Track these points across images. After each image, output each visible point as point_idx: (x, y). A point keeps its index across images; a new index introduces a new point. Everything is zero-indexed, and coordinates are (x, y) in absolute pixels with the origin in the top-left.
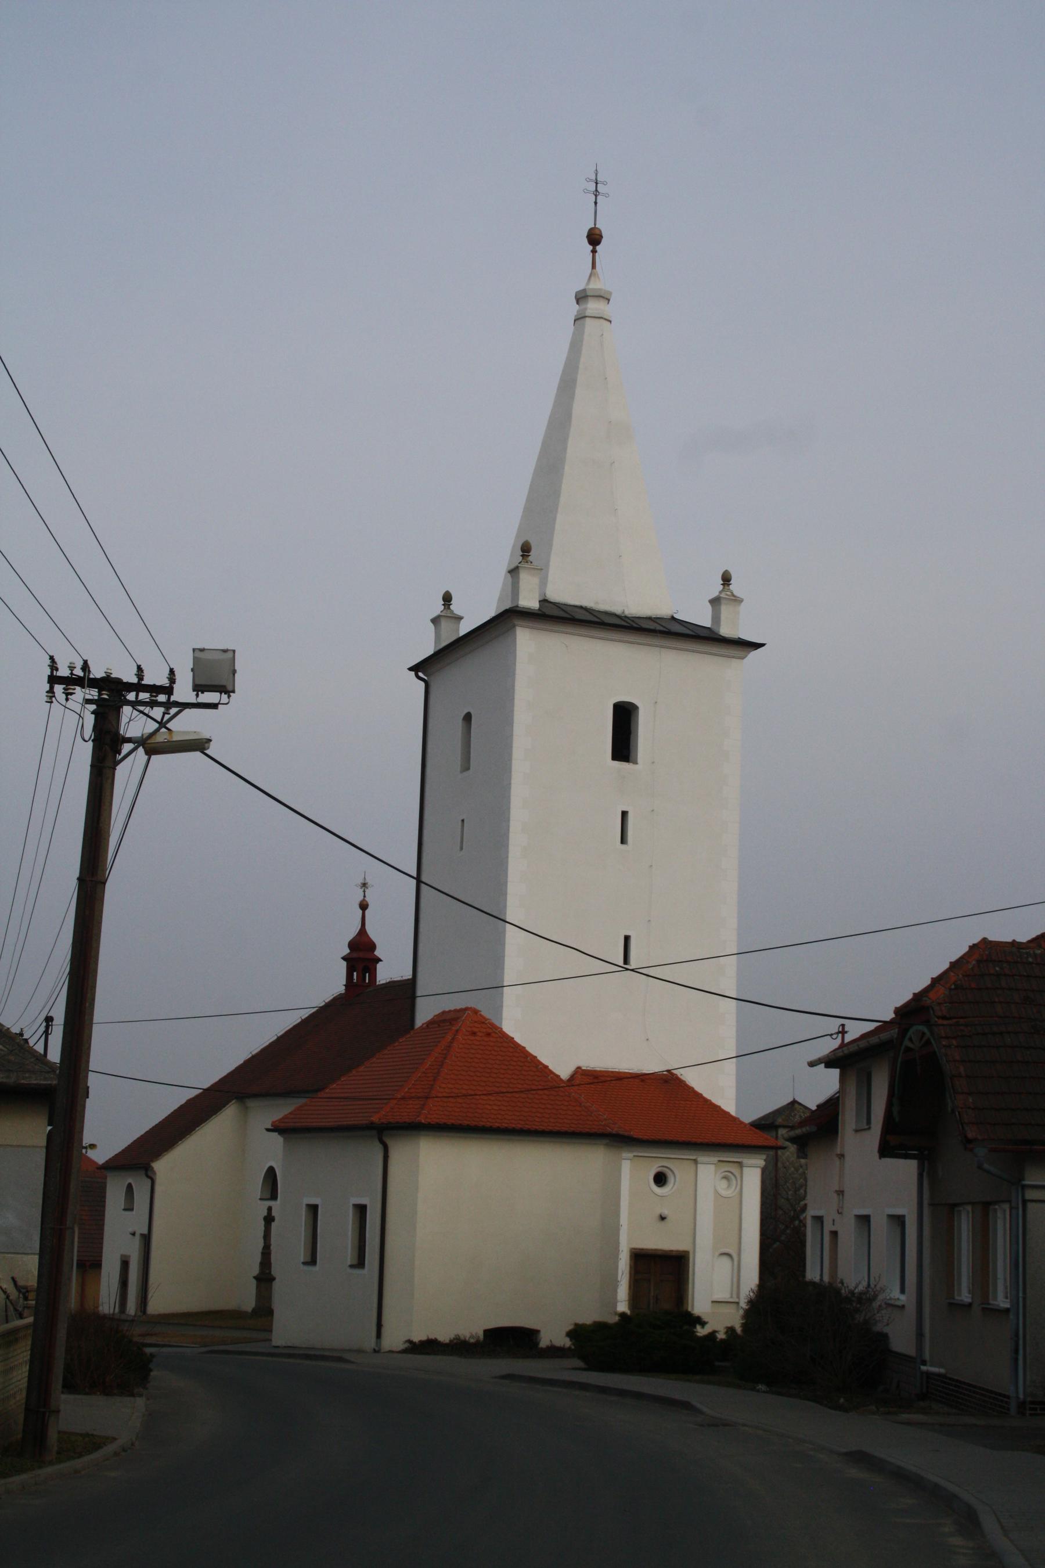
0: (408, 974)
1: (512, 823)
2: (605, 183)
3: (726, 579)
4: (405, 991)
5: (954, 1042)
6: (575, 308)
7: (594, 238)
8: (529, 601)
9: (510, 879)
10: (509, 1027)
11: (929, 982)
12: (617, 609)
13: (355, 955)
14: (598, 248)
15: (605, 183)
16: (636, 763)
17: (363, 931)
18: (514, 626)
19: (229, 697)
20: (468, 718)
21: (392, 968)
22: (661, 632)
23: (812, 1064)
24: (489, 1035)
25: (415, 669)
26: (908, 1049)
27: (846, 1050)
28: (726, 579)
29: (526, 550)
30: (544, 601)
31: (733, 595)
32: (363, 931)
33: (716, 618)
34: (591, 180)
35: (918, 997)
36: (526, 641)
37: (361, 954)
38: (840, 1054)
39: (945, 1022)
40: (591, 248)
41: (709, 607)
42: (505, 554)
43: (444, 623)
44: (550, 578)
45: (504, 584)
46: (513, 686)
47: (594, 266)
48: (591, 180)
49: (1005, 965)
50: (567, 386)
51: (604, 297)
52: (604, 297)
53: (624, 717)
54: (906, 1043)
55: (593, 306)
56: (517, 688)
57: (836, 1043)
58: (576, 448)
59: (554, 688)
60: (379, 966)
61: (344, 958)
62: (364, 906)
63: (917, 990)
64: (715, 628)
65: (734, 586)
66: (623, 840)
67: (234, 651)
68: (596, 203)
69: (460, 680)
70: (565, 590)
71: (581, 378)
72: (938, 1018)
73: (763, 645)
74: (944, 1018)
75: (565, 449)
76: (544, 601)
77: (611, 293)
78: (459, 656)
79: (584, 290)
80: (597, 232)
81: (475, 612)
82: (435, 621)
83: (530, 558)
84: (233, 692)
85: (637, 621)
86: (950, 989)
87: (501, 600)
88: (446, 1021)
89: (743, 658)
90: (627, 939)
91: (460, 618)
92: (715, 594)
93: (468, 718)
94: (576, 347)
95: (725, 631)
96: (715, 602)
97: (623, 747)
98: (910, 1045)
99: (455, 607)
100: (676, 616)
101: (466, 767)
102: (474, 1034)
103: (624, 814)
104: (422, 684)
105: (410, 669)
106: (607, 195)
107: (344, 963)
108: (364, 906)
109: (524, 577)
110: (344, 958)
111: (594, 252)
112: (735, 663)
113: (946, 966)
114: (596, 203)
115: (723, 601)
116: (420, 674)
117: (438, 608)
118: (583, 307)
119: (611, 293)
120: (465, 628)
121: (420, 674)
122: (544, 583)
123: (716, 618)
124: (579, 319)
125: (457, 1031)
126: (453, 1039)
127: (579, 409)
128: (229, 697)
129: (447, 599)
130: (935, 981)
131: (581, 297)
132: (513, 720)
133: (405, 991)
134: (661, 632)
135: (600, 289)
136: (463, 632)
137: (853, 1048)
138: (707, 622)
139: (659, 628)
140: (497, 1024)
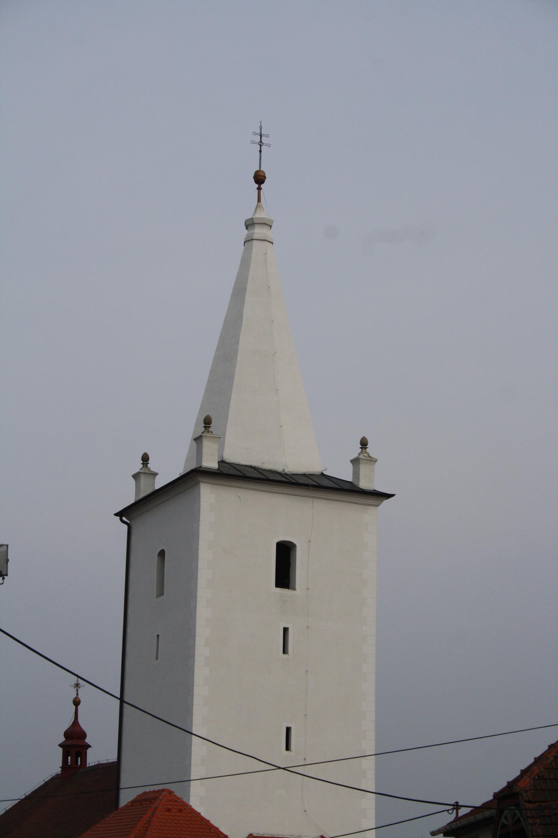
0: (113, 757)
1: (197, 639)
2: (267, 136)
3: (364, 444)
4: (112, 772)
5: (538, 821)
6: (244, 233)
7: (259, 179)
8: (210, 462)
9: (196, 683)
10: (195, 803)
11: (518, 773)
12: (279, 468)
13: (70, 742)
14: (262, 186)
15: (267, 136)
16: (294, 589)
17: (76, 723)
18: (198, 483)
19: (3, 579)
20: (162, 554)
21: (100, 752)
22: (314, 486)
23: (433, 834)
24: (180, 811)
25: (120, 514)
26: (504, 826)
27: (459, 824)
28: (364, 444)
29: (207, 422)
30: (222, 462)
31: (370, 457)
32: (76, 723)
33: (356, 474)
34: (257, 134)
35: (511, 785)
36: (208, 494)
37: (75, 742)
38: (454, 826)
39: (531, 806)
40: (257, 186)
41: (351, 466)
42: (190, 425)
43: (143, 478)
44: (226, 444)
45: (190, 449)
46: (198, 530)
47: (259, 200)
48: (257, 134)
49: (530, 816)
50: (239, 292)
51: (268, 224)
52: (268, 224)
53: (285, 553)
54: (503, 820)
55: (258, 231)
56: (201, 532)
57: (451, 817)
58: (246, 341)
59: (230, 532)
60: (89, 751)
61: (60, 745)
62: (77, 703)
63: (510, 779)
64: (355, 483)
65: (370, 449)
66: (285, 651)
67: (7, 546)
68: (260, 151)
69: (157, 526)
70: (238, 453)
71: (250, 287)
72: (525, 801)
73: (392, 495)
74: (529, 802)
75: (238, 342)
76: (222, 462)
77: (272, 221)
78: (155, 506)
79: (252, 219)
80: (262, 174)
81: (167, 471)
82: (136, 476)
83: (211, 429)
84: (7, 575)
85: (294, 477)
86: (535, 779)
87: (187, 461)
88: (147, 800)
89: (378, 506)
90: (288, 730)
91: (155, 474)
92: (355, 455)
93: (162, 554)
94: (245, 262)
95: (364, 484)
96: (355, 462)
97: (284, 577)
98: (506, 823)
99: (152, 465)
100: (325, 473)
101: (161, 592)
102: (169, 810)
103: (286, 630)
104: (125, 527)
105: (116, 515)
106: (269, 146)
107: (61, 749)
108: (77, 703)
109: (206, 444)
110: (60, 745)
111: (259, 189)
112: (371, 510)
113: (532, 760)
114: (260, 151)
115: (361, 461)
116: (124, 519)
117: (138, 466)
118: (251, 232)
119: (272, 221)
120: (160, 483)
121: (124, 519)
122: (221, 448)
123: (356, 474)
124: (248, 241)
125: (156, 808)
126: (152, 815)
127: (247, 311)
128: (3, 579)
129: (145, 459)
130: (524, 772)
131: (250, 224)
132: (198, 557)
133: (112, 772)
134: (314, 486)
135: (264, 218)
136: (158, 486)
137: (464, 822)
138: (349, 478)
139: (312, 483)
140: (185, 800)
